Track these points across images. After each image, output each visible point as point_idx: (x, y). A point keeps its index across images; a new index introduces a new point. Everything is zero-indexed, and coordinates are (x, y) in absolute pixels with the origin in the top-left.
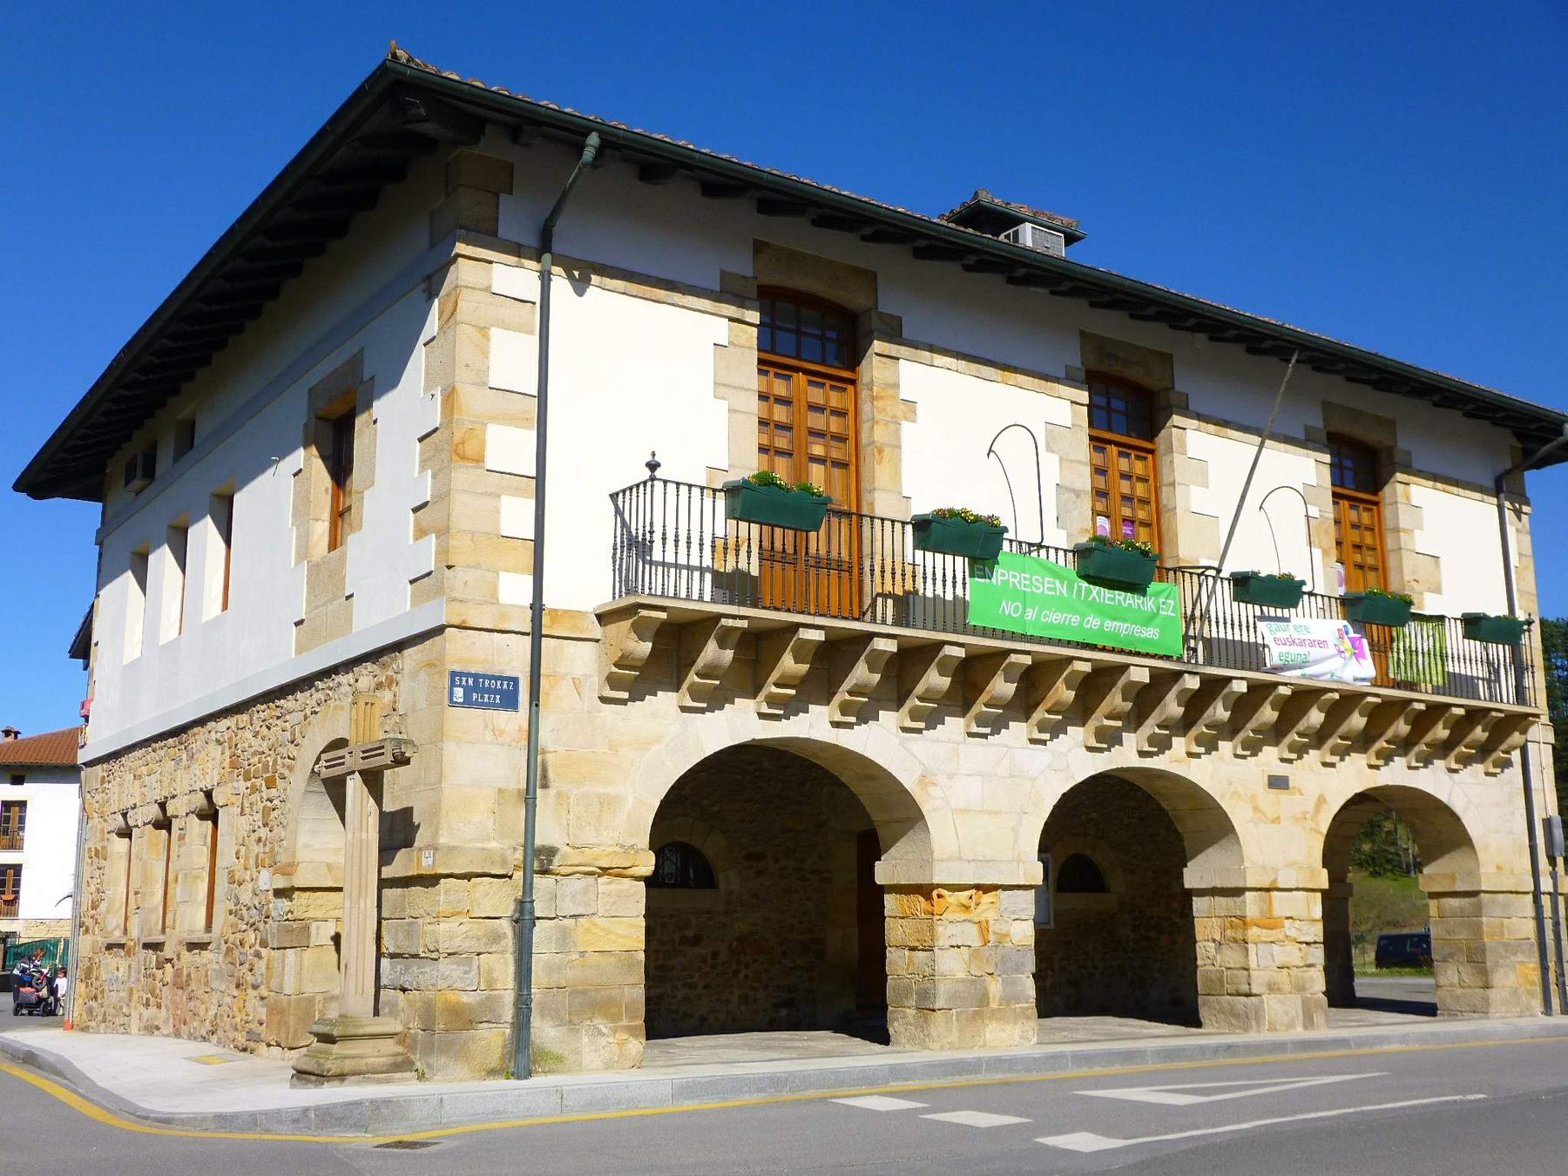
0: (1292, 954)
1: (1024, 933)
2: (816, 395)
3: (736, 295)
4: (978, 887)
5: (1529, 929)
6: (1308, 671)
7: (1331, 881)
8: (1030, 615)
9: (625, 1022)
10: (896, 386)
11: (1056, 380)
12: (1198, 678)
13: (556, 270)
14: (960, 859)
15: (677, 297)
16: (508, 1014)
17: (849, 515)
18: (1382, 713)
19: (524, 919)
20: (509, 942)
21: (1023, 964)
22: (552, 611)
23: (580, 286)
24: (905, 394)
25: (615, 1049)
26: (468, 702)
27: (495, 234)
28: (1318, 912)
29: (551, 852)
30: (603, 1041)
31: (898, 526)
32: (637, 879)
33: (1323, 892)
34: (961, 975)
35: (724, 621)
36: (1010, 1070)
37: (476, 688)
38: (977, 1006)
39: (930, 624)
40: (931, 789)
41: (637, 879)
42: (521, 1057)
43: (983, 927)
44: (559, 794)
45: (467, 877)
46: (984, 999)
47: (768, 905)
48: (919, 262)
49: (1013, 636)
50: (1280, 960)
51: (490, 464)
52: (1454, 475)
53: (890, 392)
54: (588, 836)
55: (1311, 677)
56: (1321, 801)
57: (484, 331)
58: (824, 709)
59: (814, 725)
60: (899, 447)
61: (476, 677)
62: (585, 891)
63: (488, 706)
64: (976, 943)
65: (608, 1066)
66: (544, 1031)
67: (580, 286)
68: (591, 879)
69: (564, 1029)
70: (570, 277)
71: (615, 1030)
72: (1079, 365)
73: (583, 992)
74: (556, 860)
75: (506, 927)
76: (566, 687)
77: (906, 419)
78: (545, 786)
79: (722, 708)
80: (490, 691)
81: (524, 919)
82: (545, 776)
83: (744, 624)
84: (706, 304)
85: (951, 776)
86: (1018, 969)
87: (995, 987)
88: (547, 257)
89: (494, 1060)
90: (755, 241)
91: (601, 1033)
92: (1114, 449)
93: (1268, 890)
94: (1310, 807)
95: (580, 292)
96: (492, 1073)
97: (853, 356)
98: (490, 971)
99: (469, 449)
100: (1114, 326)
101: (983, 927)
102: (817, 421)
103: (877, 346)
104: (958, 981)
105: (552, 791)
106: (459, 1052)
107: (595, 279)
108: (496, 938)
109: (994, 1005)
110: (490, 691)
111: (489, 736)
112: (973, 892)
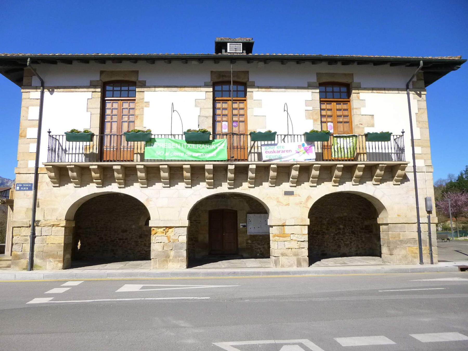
0: (294, 245)
1: (183, 239)
2: (339, 107)
3: (94, 86)
4: (167, 227)
5: (416, 235)
6: (282, 160)
7: (310, 221)
8: (167, 154)
9: (58, 259)
10: (143, 99)
11: (200, 87)
12: (234, 166)
13: (410, 92)
14: (160, 220)
15: (77, 90)
16: (28, 257)
17: (244, 135)
18: (323, 169)
19: (33, 236)
20: (29, 241)
21: (182, 247)
22: (418, 167)
23: (52, 93)
24: (145, 100)
25: (55, 265)
26: (20, 190)
27: (31, 85)
28: (306, 232)
29: (39, 221)
30: (52, 263)
31: (299, 136)
32: (62, 227)
33: (308, 225)
34: (160, 250)
35: (359, 166)
36: (148, 276)
37: (22, 186)
38: (166, 258)
39: (375, 159)
40: (150, 202)
41: (62, 227)
42: (31, 266)
43: (168, 238)
44: (42, 209)
45: (20, 227)
46: (168, 256)
47: (106, 231)
48: (375, 66)
49: (161, 161)
50: (287, 247)
51: (27, 137)
52: (198, 85)
53: (141, 101)
54: (49, 218)
55: (285, 161)
56: (309, 198)
57: (28, 108)
58: (307, 183)
59: (348, 187)
60: (143, 115)
61: (22, 184)
62: (48, 230)
63: (26, 190)
64: (167, 241)
65: (53, 269)
66: (37, 261)
67: (52, 93)
68: (50, 227)
69: (42, 260)
70: (49, 91)
71: (55, 261)
72: (316, 81)
73: (47, 253)
74: (40, 223)
75: (29, 238)
76: (44, 184)
77: (146, 107)
78: (38, 207)
79: (300, 185)
80: (25, 187)
81: (33, 236)
82: (38, 205)
83: (342, 166)
84: (85, 90)
85: (157, 198)
86: (181, 248)
87: (172, 253)
88: (408, 90)
89: (25, 267)
90: (317, 73)
91: (51, 262)
92: (335, 103)
93: (283, 226)
94: (304, 200)
95: (51, 94)
96: (24, 269)
97: (349, 95)
98: (25, 247)
99: (23, 135)
100: (325, 68)
101: (168, 238)
102: (339, 113)
103: (353, 91)
104: (159, 252)
105: (40, 208)
106: (16, 264)
107: (55, 90)
108: (26, 240)
109: (171, 258)
110: (25, 187)
111: (25, 196)
112: (165, 228)
